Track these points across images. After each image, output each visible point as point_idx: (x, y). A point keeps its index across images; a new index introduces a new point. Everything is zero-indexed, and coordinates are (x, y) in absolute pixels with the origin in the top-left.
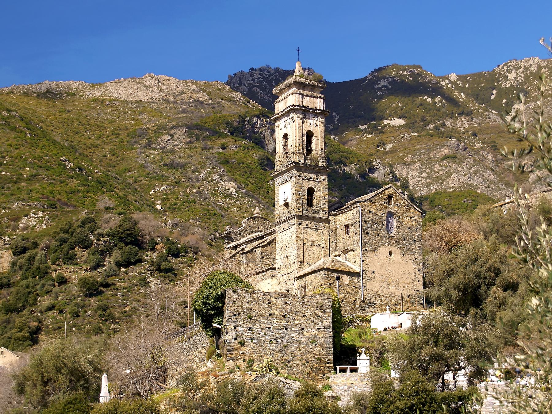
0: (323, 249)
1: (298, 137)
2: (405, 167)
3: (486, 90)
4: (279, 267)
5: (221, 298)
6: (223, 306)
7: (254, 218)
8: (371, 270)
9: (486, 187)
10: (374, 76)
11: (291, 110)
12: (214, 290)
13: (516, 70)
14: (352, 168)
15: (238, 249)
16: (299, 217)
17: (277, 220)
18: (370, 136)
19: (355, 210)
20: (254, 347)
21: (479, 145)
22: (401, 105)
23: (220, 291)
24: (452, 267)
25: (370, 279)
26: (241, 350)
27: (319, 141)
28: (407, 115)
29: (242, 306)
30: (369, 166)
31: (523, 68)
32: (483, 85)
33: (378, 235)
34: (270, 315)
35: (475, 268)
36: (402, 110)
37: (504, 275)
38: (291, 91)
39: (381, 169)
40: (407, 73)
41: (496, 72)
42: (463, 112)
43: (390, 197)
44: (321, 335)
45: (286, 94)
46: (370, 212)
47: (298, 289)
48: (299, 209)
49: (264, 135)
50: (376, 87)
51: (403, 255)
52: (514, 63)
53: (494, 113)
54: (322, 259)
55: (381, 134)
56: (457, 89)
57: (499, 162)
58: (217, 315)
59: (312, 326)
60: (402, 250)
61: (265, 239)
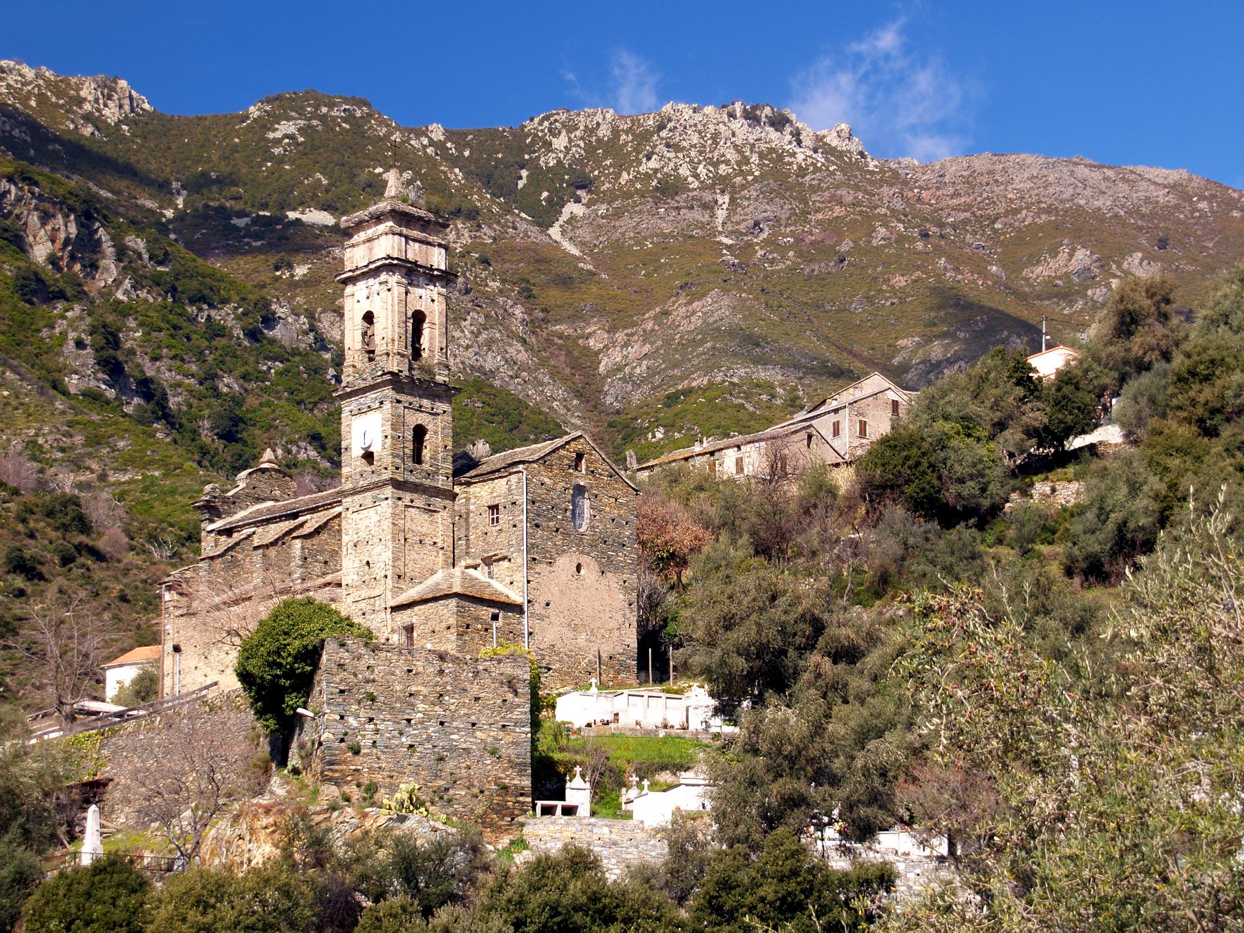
0: (441, 552)
1: (397, 322)
2: (338, 319)
3: (507, 167)
4: (349, 582)
5: (312, 655)
6: (313, 672)
7: (264, 471)
8: (542, 600)
9: (511, 377)
10: (266, 111)
11: (384, 265)
12: (295, 639)
13: (569, 132)
14: (228, 314)
15: (237, 537)
16: (398, 485)
17: (348, 486)
18: (259, 243)
19: (514, 478)
20: (378, 758)
21: (495, 285)
22: (325, 182)
23: (311, 641)
24: (734, 611)
25: (541, 618)
26: (351, 763)
27: (437, 332)
28: (338, 205)
29: (355, 675)
30: (263, 313)
31: (582, 128)
32: (500, 156)
33: (557, 530)
34: (411, 695)
35: (776, 613)
36: (327, 191)
37: (832, 631)
38: (382, 227)
39: (290, 320)
40: (338, 114)
41: (526, 130)
42: (459, 211)
43: (580, 456)
44: (509, 739)
45: (370, 232)
46: (542, 484)
47: (393, 631)
48: (397, 468)
49: (26, 224)
50: (271, 135)
51: (603, 573)
52: (563, 117)
53: (525, 219)
54: (440, 571)
55: (284, 242)
56: (446, 160)
57: (537, 324)
58: (295, 688)
59: (491, 721)
60: (600, 564)
61: (301, 519)
